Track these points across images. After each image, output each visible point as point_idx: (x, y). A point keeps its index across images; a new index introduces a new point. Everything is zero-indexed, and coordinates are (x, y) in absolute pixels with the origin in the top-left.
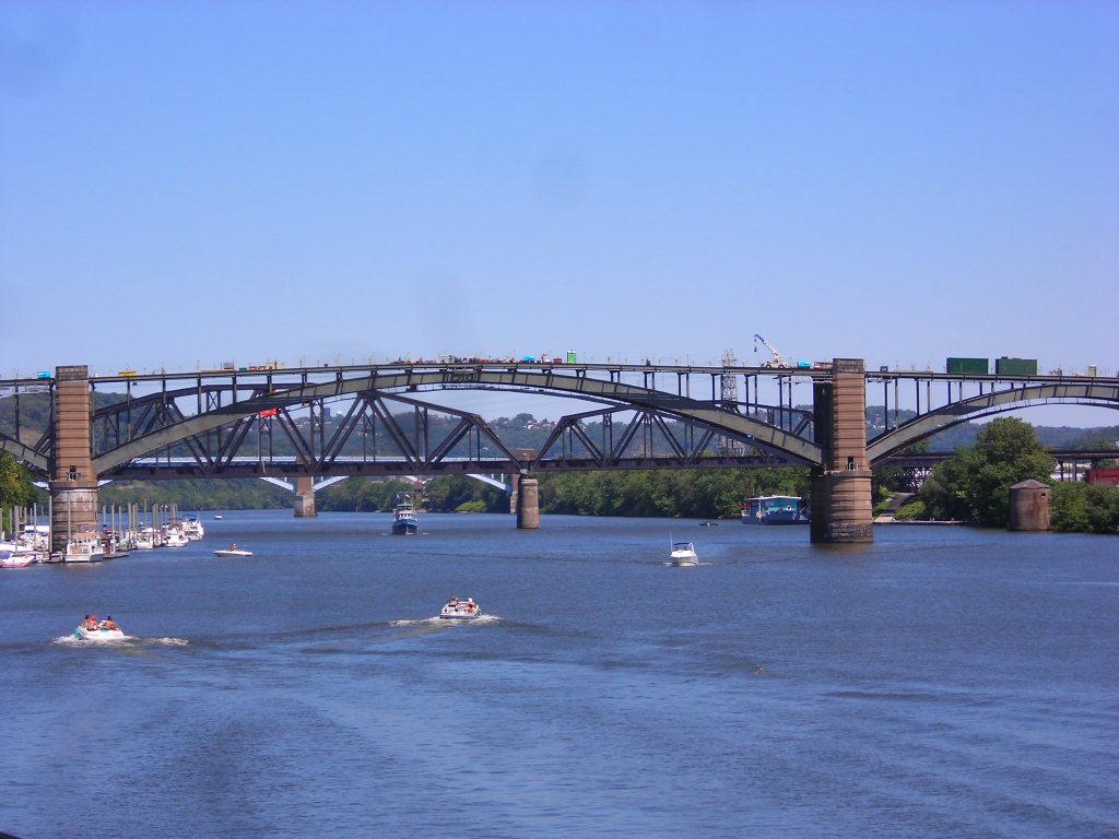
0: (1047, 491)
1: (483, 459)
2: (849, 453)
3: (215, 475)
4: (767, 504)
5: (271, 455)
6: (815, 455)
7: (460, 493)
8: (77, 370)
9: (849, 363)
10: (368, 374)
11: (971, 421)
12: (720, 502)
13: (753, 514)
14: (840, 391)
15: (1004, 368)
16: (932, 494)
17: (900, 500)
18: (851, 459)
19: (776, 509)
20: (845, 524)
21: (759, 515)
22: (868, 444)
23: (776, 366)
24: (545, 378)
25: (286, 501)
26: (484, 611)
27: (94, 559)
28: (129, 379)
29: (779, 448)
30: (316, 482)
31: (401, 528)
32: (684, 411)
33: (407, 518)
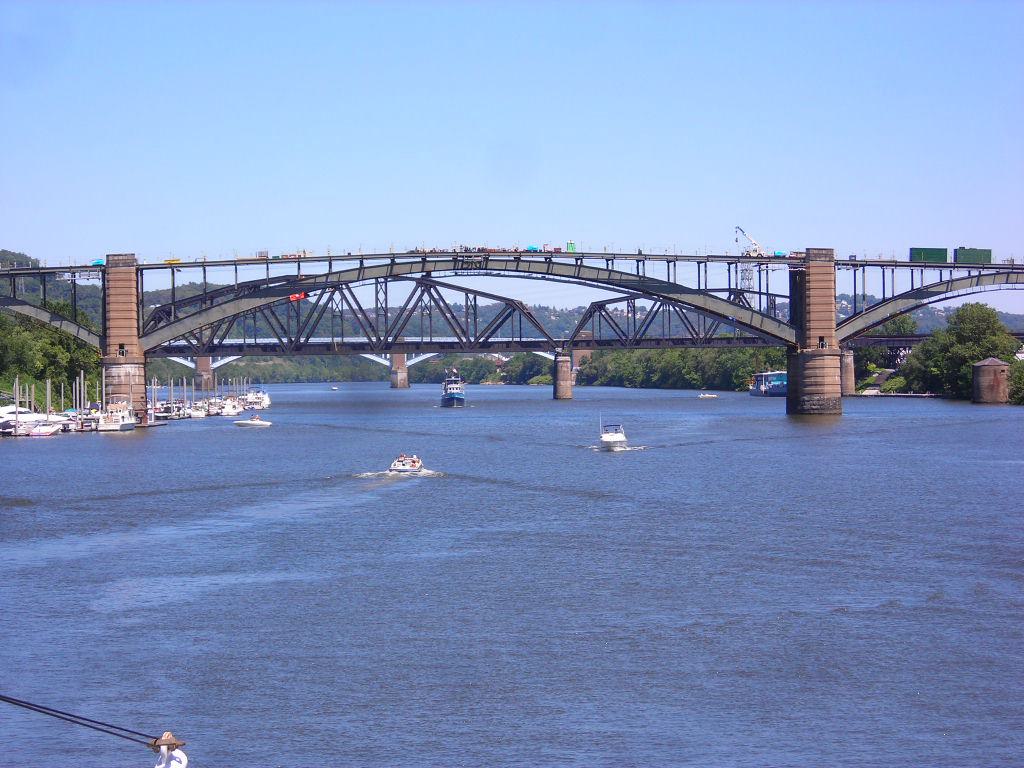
0: (1005, 368)
1: (524, 340)
2: (821, 333)
3: (294, 352)
4: (770, 379)
5: (333, 337)
6: (789, 335)
7: (533, 366)
8: (124, 258)
9: (821, 252)
10: (388, 261)
11: (930, 305)
12: (737, 377)
13: (758, 387)
14: (812, 278)
15: (961, 258)
16: (912, 370)
17: (886, 375)
18: (821, 339)
19: (777, 383)
20: (816, 398)
21: (763, 388)
22: (838, 325)
23: (755, 255)
24: (546, 265)
25: (387, 375)
26: (426, 466)
27: (124, 428)
28: (264, 260)
29: (757, 329)
30: (213, 361)
31: (449, 401)
32: (671, 296)
33: (455, 391)
